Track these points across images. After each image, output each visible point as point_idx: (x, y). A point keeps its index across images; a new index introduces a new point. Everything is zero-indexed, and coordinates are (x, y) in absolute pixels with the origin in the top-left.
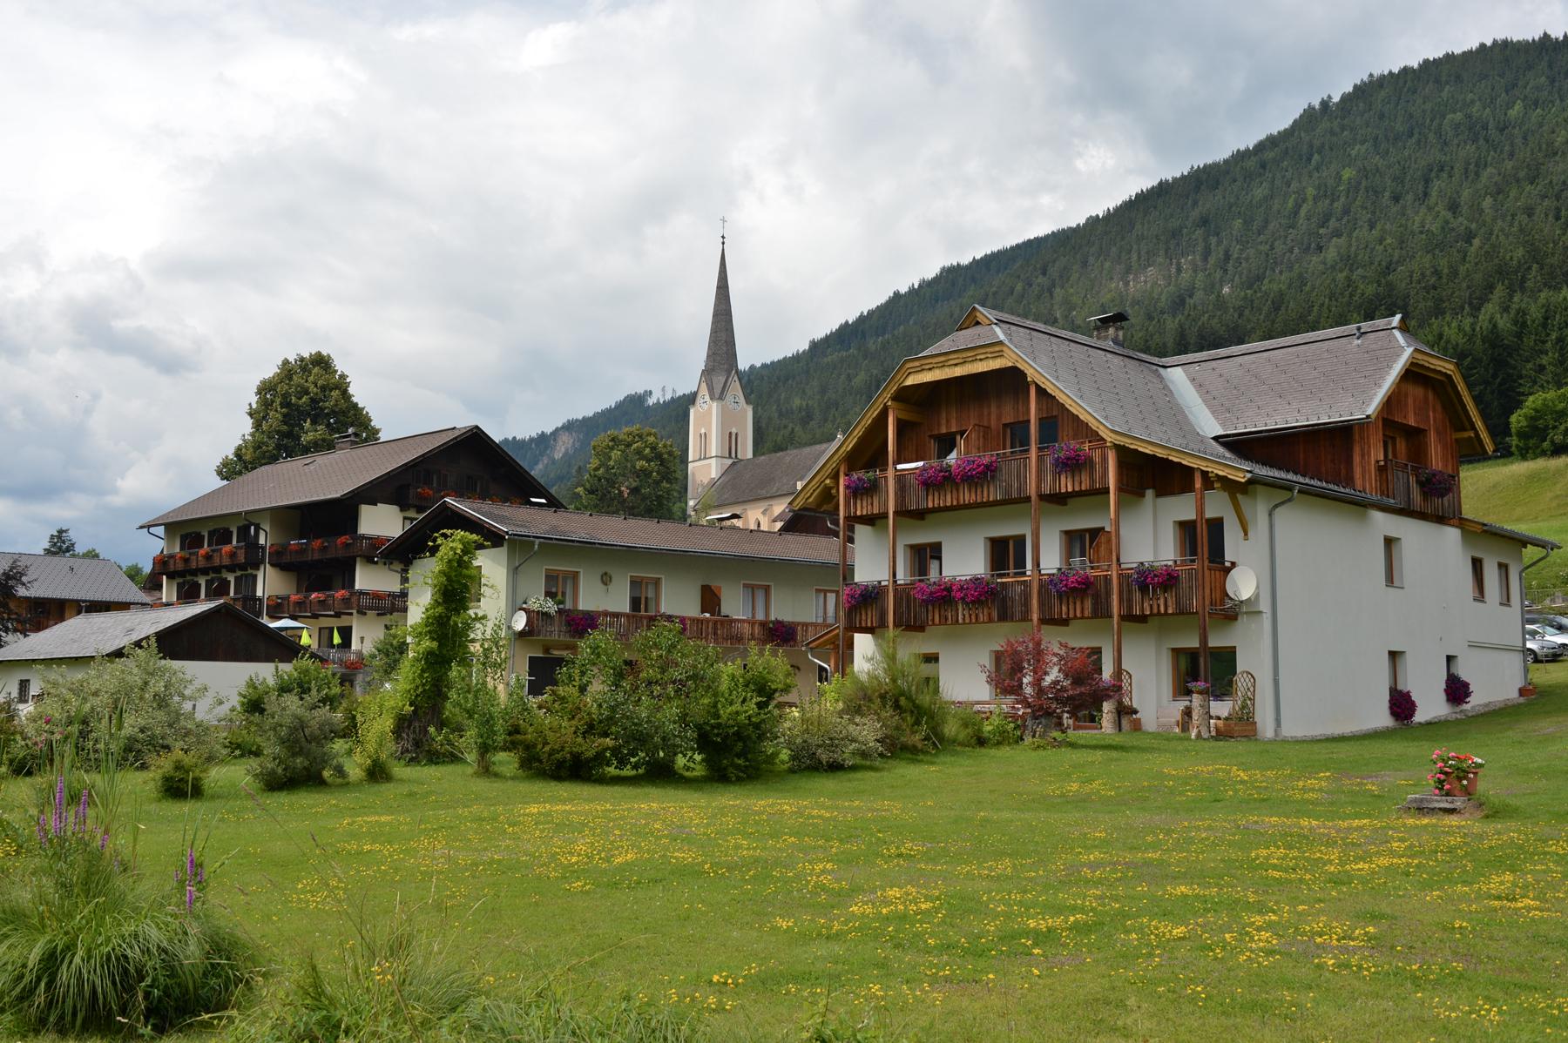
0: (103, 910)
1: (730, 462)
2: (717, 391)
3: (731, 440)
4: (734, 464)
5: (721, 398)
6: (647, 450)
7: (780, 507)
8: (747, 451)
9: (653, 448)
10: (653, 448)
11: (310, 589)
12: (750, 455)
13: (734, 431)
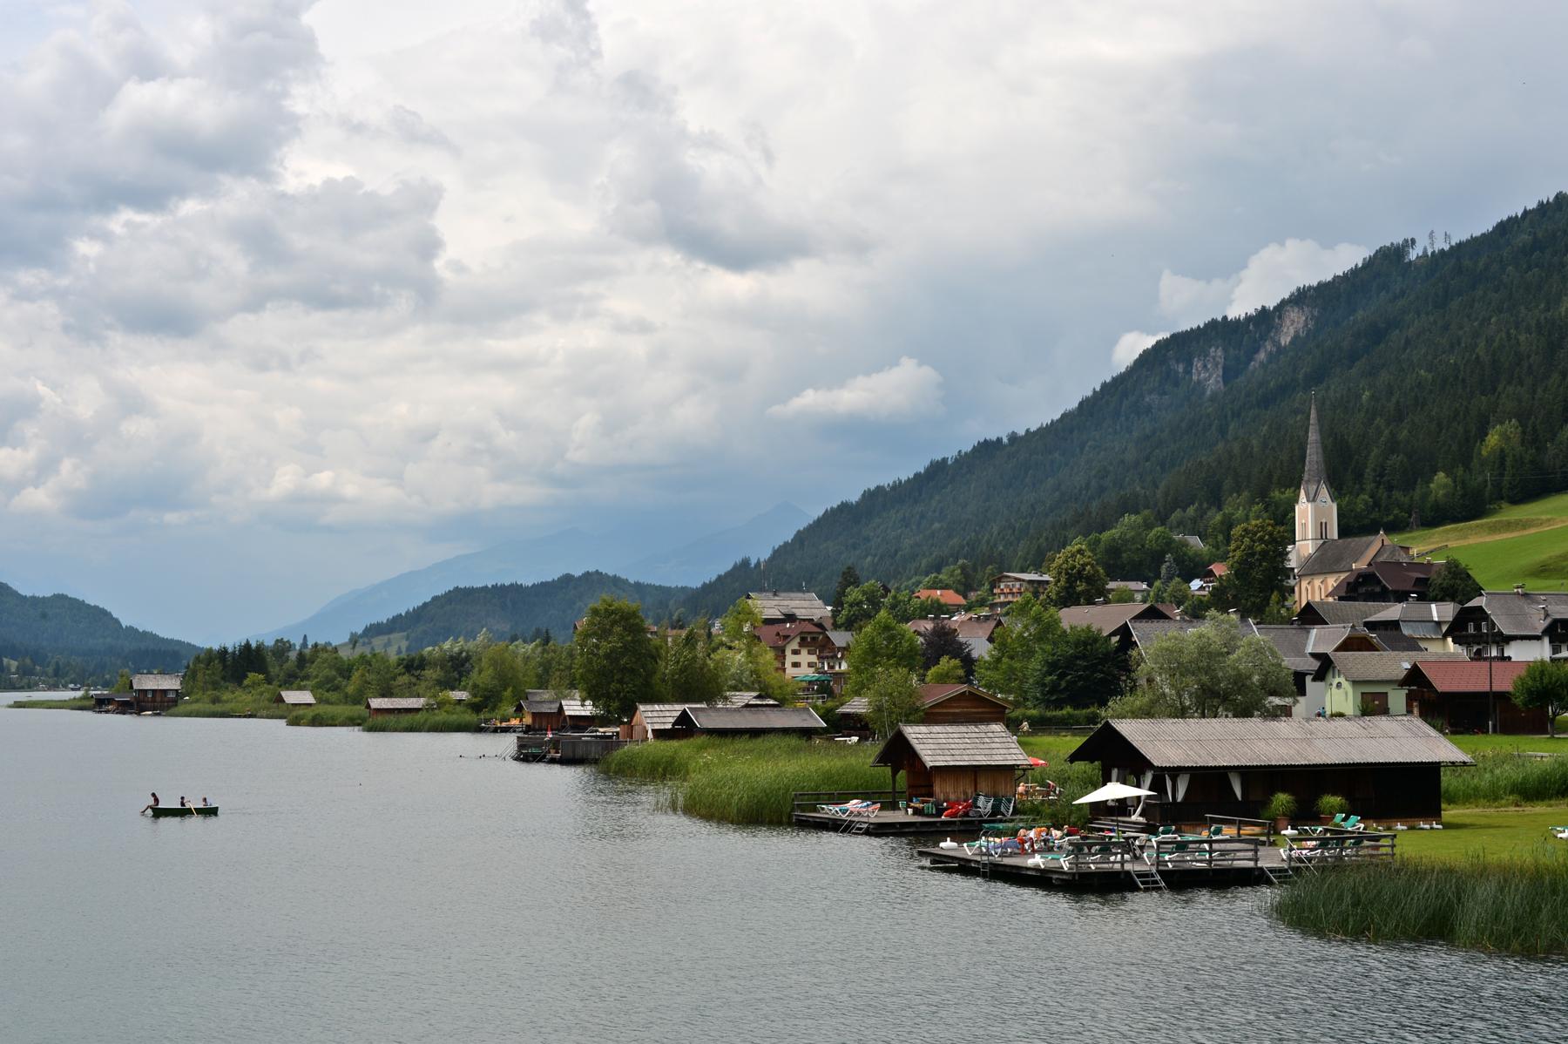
3: (1322, 528)
5: (1314, 500)
7: (1332, 582)
9: (1271, 534)
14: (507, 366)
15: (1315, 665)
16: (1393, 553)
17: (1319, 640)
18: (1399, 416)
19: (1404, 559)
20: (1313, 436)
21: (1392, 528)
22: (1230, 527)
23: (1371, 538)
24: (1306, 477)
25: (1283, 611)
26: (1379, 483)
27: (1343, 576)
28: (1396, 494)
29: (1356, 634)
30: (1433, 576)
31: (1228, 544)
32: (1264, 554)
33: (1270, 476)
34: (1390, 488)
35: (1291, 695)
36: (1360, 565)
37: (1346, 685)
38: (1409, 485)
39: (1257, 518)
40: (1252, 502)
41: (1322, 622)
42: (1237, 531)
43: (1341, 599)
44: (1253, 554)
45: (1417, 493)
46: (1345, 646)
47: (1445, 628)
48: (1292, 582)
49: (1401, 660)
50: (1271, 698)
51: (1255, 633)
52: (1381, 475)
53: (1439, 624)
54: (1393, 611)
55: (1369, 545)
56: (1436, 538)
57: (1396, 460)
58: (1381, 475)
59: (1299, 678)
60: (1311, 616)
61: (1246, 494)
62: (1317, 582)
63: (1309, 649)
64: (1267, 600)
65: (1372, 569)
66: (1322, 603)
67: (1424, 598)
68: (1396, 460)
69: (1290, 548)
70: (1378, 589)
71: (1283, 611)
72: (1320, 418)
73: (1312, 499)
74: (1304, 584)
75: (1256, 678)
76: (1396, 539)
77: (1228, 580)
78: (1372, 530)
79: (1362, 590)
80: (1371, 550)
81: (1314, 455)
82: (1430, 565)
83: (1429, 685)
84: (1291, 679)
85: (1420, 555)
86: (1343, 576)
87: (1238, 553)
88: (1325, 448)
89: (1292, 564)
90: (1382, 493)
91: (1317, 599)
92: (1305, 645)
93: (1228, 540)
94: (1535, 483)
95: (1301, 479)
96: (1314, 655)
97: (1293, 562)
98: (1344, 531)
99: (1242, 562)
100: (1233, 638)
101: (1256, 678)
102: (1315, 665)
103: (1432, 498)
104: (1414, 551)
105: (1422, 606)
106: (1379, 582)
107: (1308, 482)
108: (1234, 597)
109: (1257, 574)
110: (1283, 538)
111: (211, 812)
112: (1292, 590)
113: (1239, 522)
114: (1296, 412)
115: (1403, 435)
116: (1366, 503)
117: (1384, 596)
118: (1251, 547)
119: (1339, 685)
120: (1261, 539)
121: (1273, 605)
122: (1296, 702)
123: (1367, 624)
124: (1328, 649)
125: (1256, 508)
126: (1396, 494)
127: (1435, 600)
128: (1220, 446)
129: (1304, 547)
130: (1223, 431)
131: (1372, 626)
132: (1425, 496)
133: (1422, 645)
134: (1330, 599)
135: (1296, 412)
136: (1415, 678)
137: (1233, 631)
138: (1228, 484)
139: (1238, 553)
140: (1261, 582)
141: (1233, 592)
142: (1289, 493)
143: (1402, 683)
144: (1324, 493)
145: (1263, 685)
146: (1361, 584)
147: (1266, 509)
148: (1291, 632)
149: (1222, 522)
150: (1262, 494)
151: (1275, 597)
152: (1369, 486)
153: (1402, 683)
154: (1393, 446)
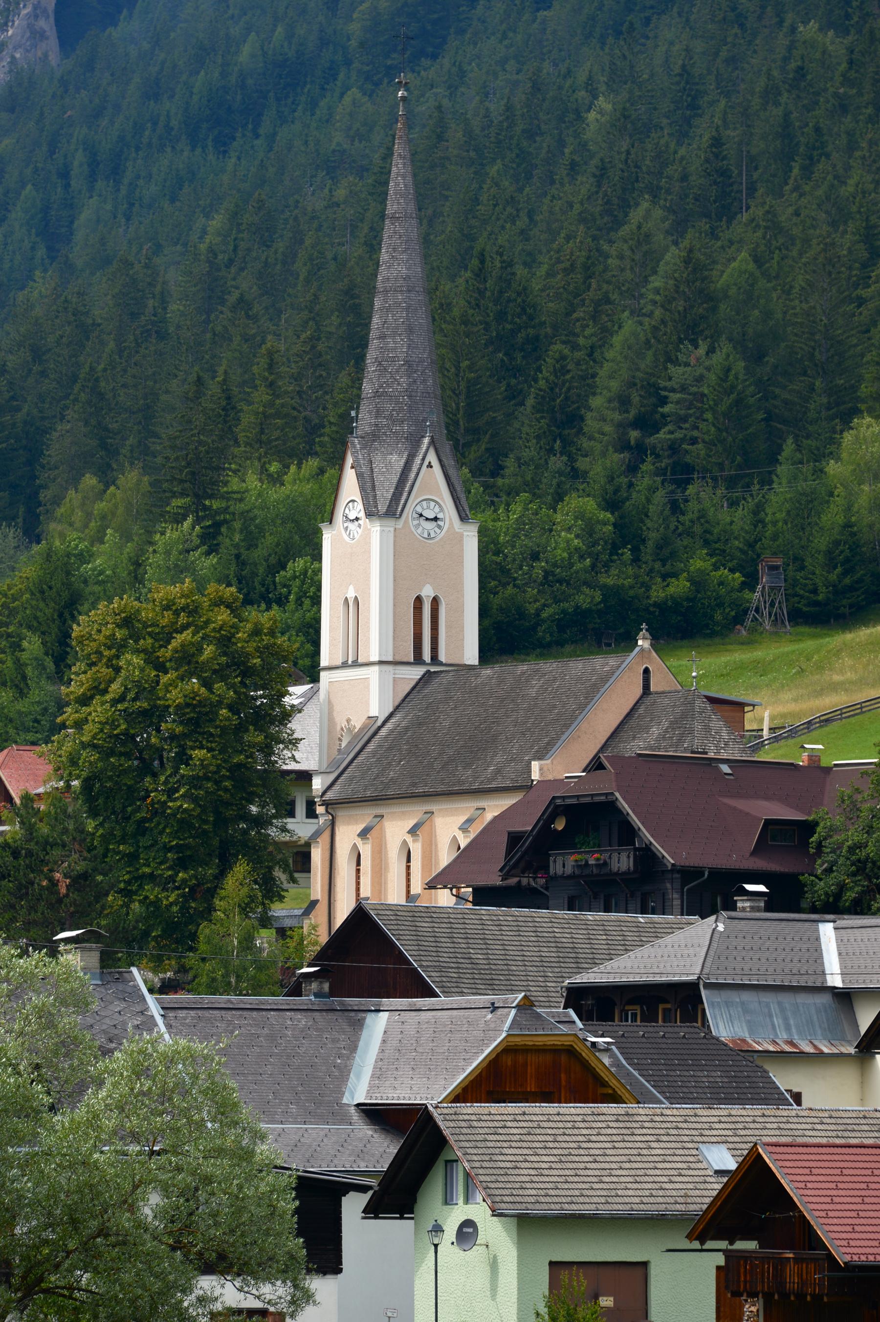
0: (350, 129)
1: (416, 673)
2: (385, 494)
3: (422, 618)
4: (427, 677)
5: (393, 512)
6: (209, 650)
7: (452, 828)
8: (464, 642)
9: (225, 641)
10: (225, 641)
11: (605, 509)
12: (471, 655)
13: (427, 593)
14: (834, 687)
15: (379, 1151)
16: (681, 723)
17: (398, 1055)
18: (720, 200)
19: (722, 746)
20: (397, 264)
21: (685, 625)
22: (70, 606)
23: (601, 663)
24: (365, 419)
25: (264, 939)
26: (640, 451)
27: (494, 807)
28: (703, 496)
29: (539, 1036)
30: (828, 815)
31: (60, 675)
32: (197, 717)
33: (229, 408)
34: (681, 474)
35: (288, 1271)
36: (560, 767)
37: (495, 1233)
38: (750, 466)
39: (176, 573)
40: (154, 512)
41: (416, 987)
42: (92, 625)
43: (484, 896)
44: (152, 716)
45: (780, 496)
46: (500, 1079)
47: (865, 1020)
48: (300, 827)
49: (704, 1138)
50: (206, 1284)
51: (155, 1025)
52: (647, 423)
53: (845, 998)
54: (675, 948)
55: (593, 690)
56: (845, 671)
57: (703, 365)
58: (647, 423)
59: (318, 1201)
60: (367, 960)
61: (132, 479)
62: (396, 828)
63: (359, 1090)
64: (204, 895)
65: (604, 785)
66: (413, 912)
67: (788, 897)
68: (703, 365)
69: (296, 693)
70: (622, 862)
71: (264, 939)
72: (424, 194)
73: (387, 507)
74: (347, 835)
75: (152, 1203)
76: (696, 670)
77: (60, 815)
78: (605, 627)
79: (564, 863)
80: (602, 709)
81: (396, 342)
82: (818, 771)
83: (804, 1235)
84: (289, 1204)
85: (780, 734)
86: (494, 807)
87: (98, 711)
88: (440, 311)
89: (305, 757)
90: (648, 490)
91: (395, 896)
92: (342, 1075)
93: (61, 655)
94: (823, 611)
95: (346, 425)
96: (378, 1115)
97: (308, 749)
98: (503, 636)
99: (117, 744)
100: (68, 1045)
101: (152, 1203)
102: (379, 1151)
103: (832, 517)
104: (763, 718)
105: (783, 928)
106: (627, 833)
107: (373, 438)
108: (79, 881)
109: (173, 795)
110: (271, 653)
111: (646, 671)
112: (301, 859)
113: (109, 588)
114: (332, 166)
115: (732, 270)
116: (589, 530)
117: (647, 888)
118: (145, 689)
119: (467, 1233)
120: (187, 659)
121: (225, 924)
122: (302, 1298)
123: (582, 999)
124: (429, 1090)
125: (169, 536)
126: (703, 496)
127: (832, 907)
128: (42, 285)
129: (348, 696)
130: (53, 232)
131: (597, 1003)
132: (807, 508)
133: (784, 1079)
134: (444, 898)
135: (332, 166)
136: (752, 1204)
137: (68, 1020)
138: (64, 438)
139: (98, 711)
140: (184, 824)
141: (77, 863)
142: (297, 482)
143: (709, 1226)
144: (433, 486)
145: (180, 1231)
146: (564, 841)
147: (210, 539)
148: (294, 1024)
149: (41, 590)
150: (196, 483)
151: (237, 880)
152: (601, 463)
153: (709, 1226)
154: (694, 316)
